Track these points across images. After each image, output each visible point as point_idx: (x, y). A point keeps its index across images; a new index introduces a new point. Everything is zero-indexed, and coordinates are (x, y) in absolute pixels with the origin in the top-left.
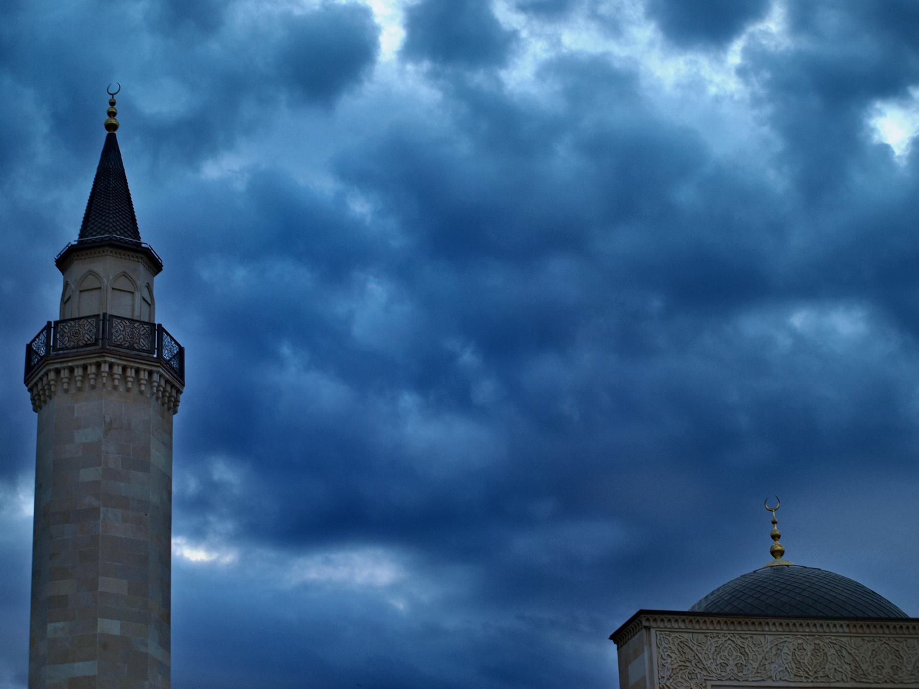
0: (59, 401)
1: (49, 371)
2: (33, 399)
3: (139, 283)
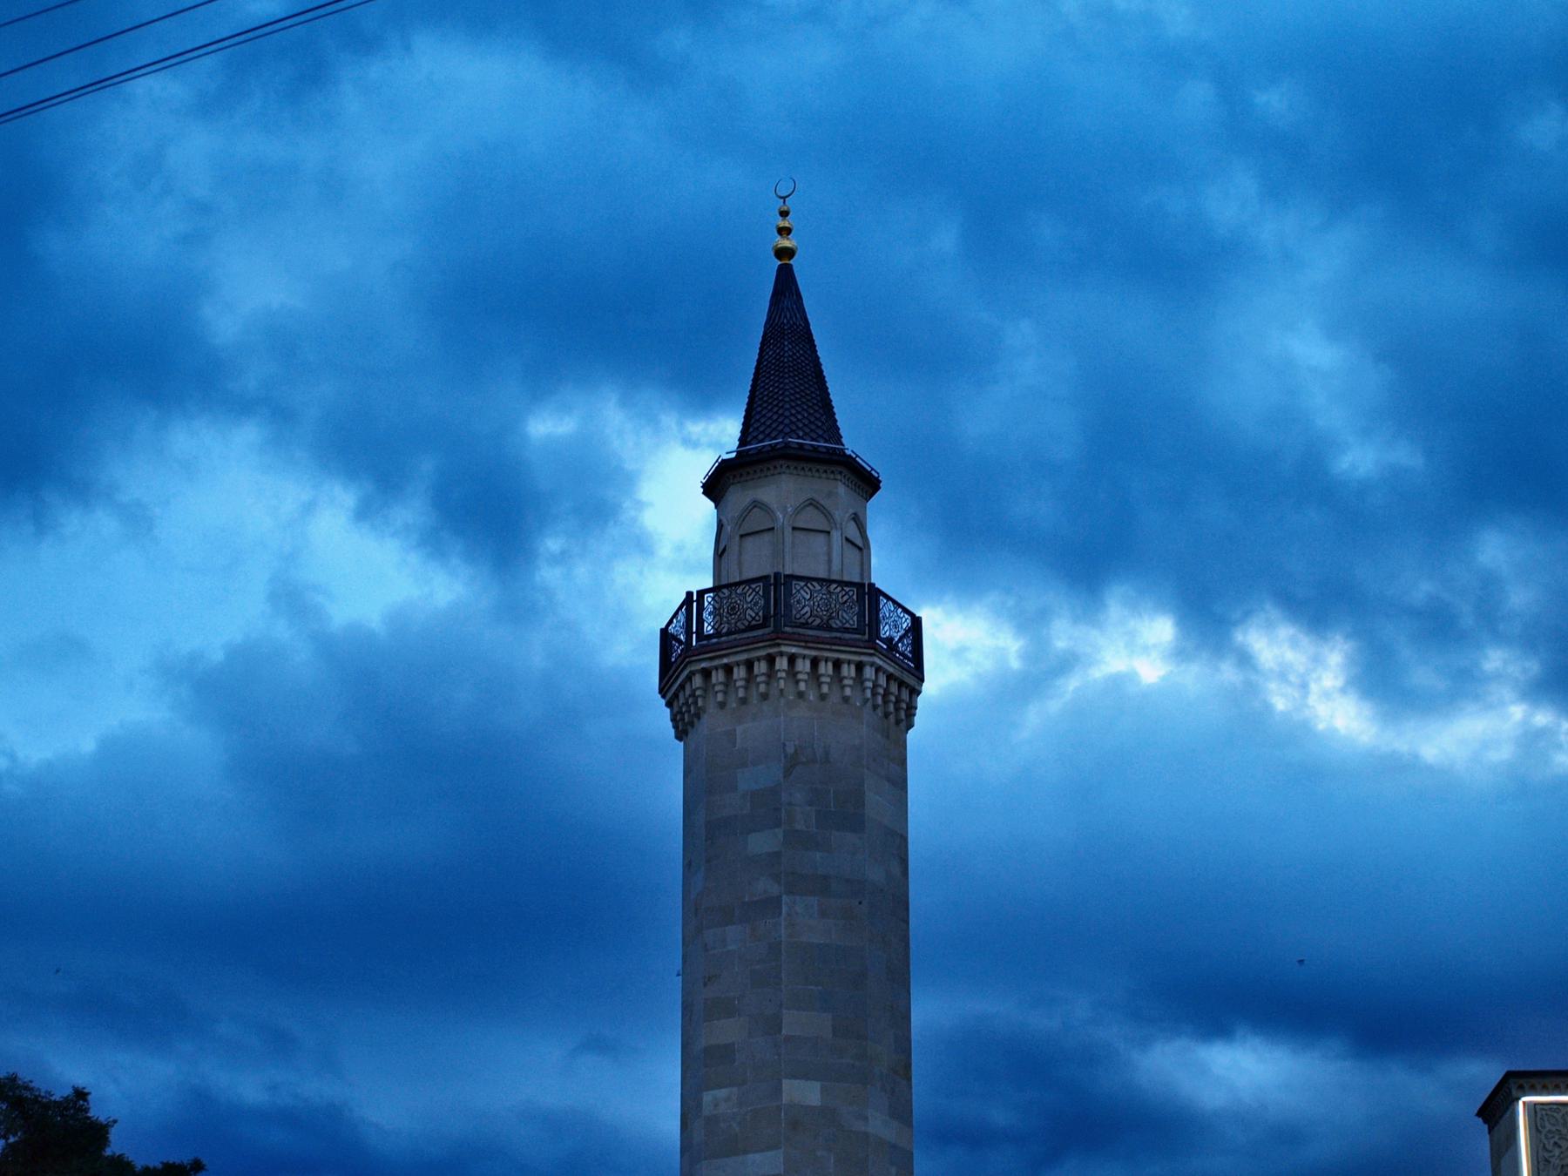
0: (712, 722)
1: (693, 673)
2: (673, 719)
3: (838, 515)
